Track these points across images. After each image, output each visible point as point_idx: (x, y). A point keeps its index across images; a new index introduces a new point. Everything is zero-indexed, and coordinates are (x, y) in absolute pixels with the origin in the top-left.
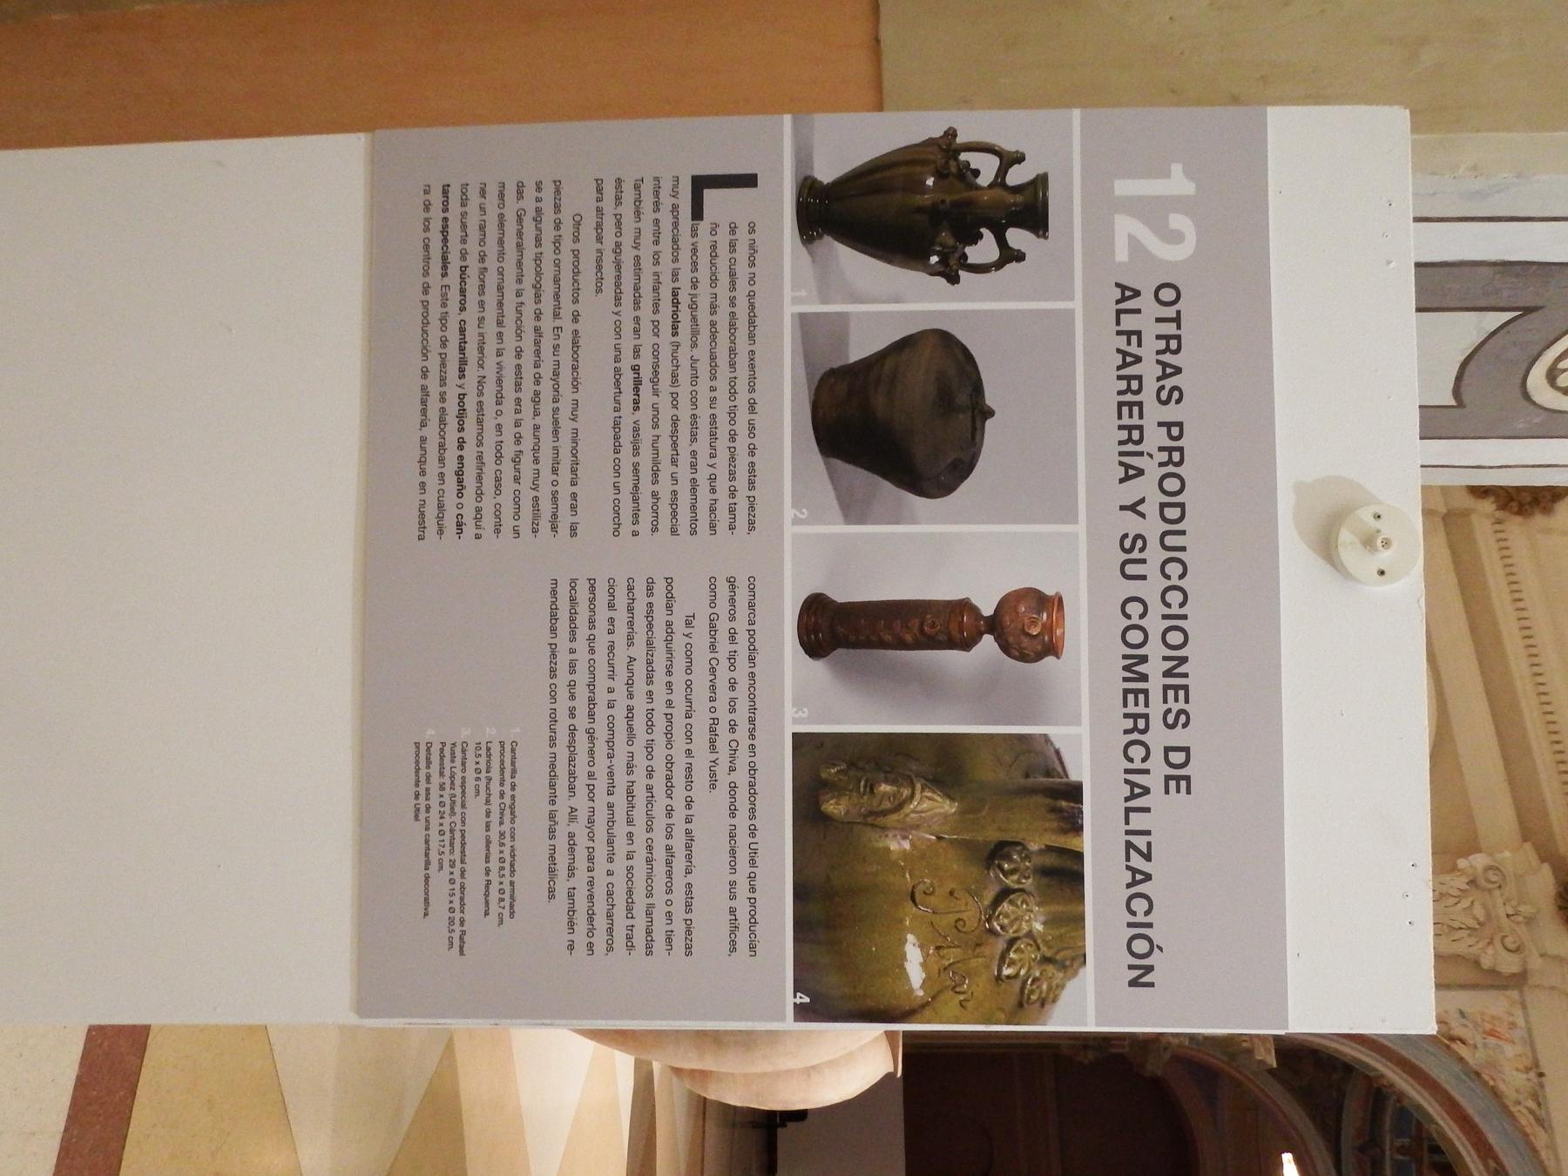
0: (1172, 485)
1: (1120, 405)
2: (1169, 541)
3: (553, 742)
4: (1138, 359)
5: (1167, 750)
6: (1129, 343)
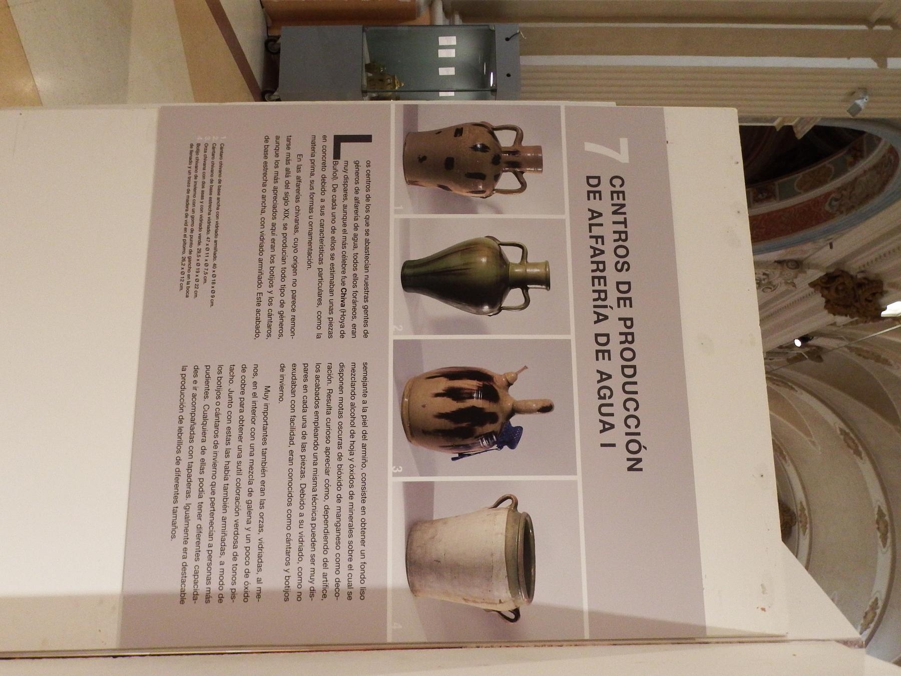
0: (628, 354)
1: (593, 278)
2: (628, 388)
3: (221, 164)
4: (602, 252)
5: (618, 283)
6: (597, 243)
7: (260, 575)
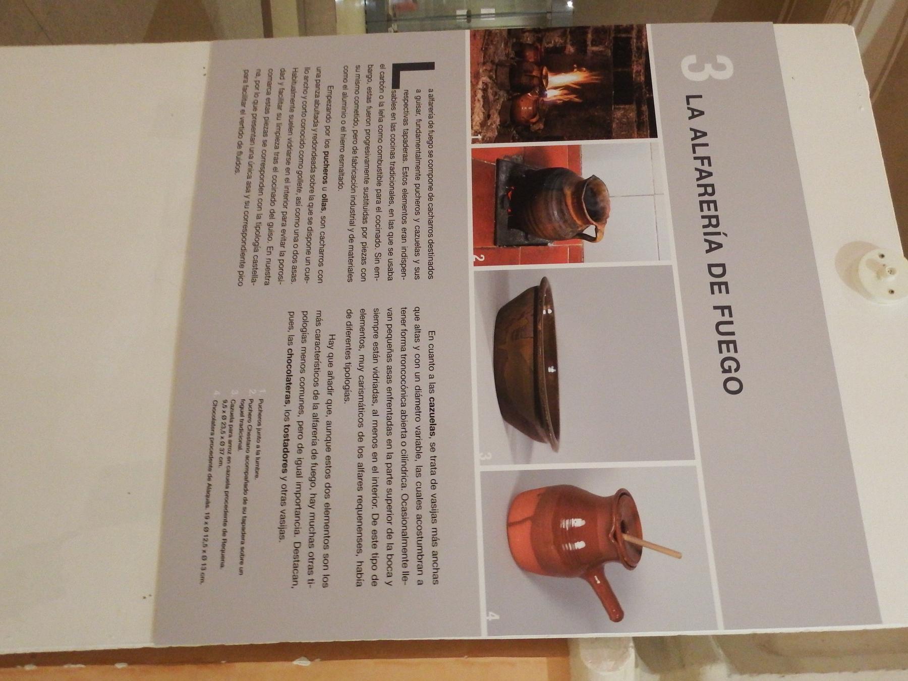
1: (701, 203)
4: (710, 174)
6: (703, 164)
7: (330, 418)
